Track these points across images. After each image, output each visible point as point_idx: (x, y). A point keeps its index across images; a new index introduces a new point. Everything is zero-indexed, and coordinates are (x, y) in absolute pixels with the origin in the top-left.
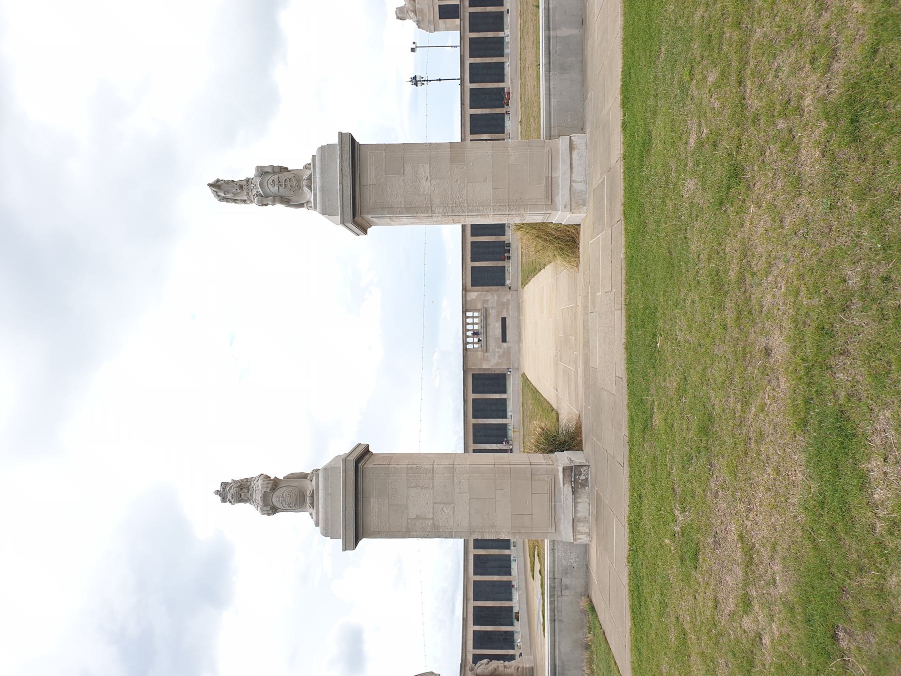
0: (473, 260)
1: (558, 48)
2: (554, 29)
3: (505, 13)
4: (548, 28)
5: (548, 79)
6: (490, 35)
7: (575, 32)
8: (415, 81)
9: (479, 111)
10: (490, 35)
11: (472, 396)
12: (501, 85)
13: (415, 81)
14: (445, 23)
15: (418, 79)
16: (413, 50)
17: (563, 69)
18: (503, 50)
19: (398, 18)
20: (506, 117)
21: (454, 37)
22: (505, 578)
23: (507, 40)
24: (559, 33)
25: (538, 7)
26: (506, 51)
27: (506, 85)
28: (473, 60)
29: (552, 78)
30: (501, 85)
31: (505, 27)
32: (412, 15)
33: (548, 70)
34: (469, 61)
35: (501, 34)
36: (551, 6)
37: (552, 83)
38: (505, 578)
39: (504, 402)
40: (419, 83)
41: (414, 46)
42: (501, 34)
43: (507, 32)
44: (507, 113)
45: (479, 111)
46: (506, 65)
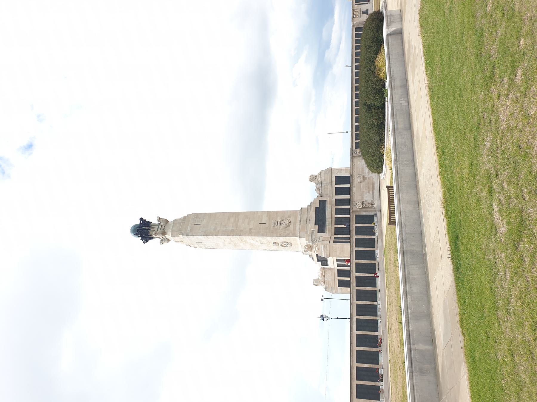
0: (358, 379)
1: (417, 357)
2: (414, 344)
3: (378, 291)
4: (409, 343)
5: (412, 378)
6: (369, 303)
7: (428, 347)
8: (322, 318)
9: (362, 349)
10: (369, 303)
11: (356, 365)
12: (376, 333)
13: (322, 318)
14: (342, 290)
15: (324, 317)
16: (322, 300)
17: (422, 372)
18: (377, 312)
19: (314, 284)
20: (380, 354)
21: (348, 296)
22: (373, 262)
23: (379, 307)
24: (417, 347)
25: (402, 323)
26: (379, 313)
27: (379, 333)
28: (358, 317)
29: (414, 377)
30: (376, 333)
31: (378, 299)
32: (323, 284)
33: (411, 372)
34: (356, 382)
35: (375, 303)
36: (410, 329)
37: (414, 381)
38: (373, 262)
39: (376, 322)
40: (325, 319)
41: (323, 298)
42: (375, 303)
43: (379, 302)
44: (380, 351)
45: (361, 317)
46: (379, 322)
